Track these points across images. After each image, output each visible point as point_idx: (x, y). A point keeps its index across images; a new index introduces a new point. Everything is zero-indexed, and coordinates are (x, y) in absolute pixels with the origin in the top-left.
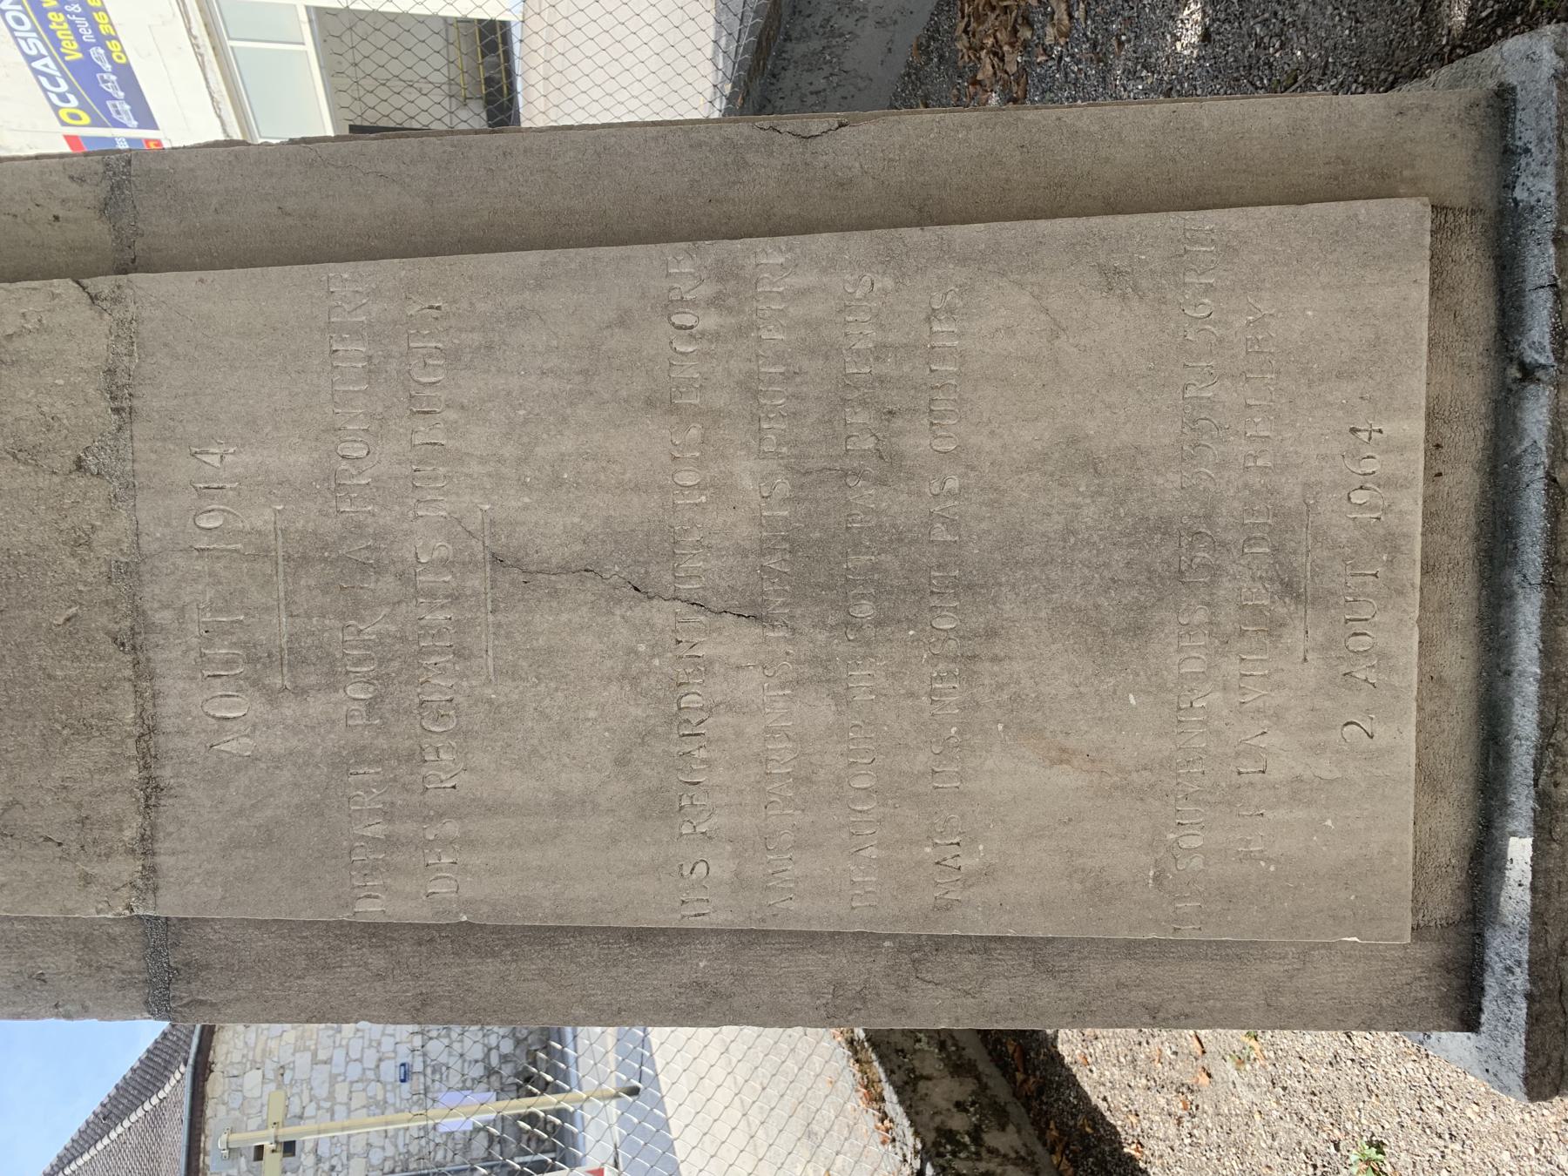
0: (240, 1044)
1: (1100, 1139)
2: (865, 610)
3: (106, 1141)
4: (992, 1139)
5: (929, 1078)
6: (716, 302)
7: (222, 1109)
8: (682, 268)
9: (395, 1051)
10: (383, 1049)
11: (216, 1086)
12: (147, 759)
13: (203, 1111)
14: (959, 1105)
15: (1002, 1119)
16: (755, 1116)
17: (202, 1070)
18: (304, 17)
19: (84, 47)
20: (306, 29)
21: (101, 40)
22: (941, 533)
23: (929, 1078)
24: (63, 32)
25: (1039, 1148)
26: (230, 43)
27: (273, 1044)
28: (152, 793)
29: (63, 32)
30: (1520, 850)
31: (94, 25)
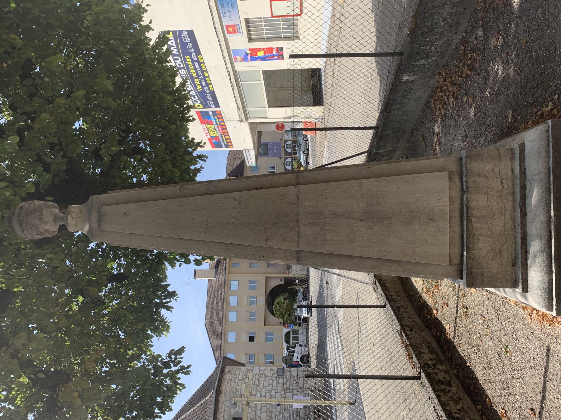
0: (229, 386)
1: (463, 364)
2: (375, 220)
3: (190, 411)
4: (438, 367)
5: (424, 353)
6: (358, 186)
7: (223, 406)
8: (354, 183)
9: (275, 395)
10: (272, 394)
11: (222, 398)
12: (298, 234)
13: (218, 406)
14: (431, 359)
15: (442, 363)
16: (390, 397)
17: (218, 393)
18: (261, 73)
19: (203, 87)
20: (262, 76)
21: (207, 85)
22: (384, 211)
23: (424, 353)
24: (198, 84)
25: (450, 370)
26: (241, 83)
27: (239, 387)
28: (299, 237)
29: (198, 84)
30: (465, 253)
31: (206, 81)
